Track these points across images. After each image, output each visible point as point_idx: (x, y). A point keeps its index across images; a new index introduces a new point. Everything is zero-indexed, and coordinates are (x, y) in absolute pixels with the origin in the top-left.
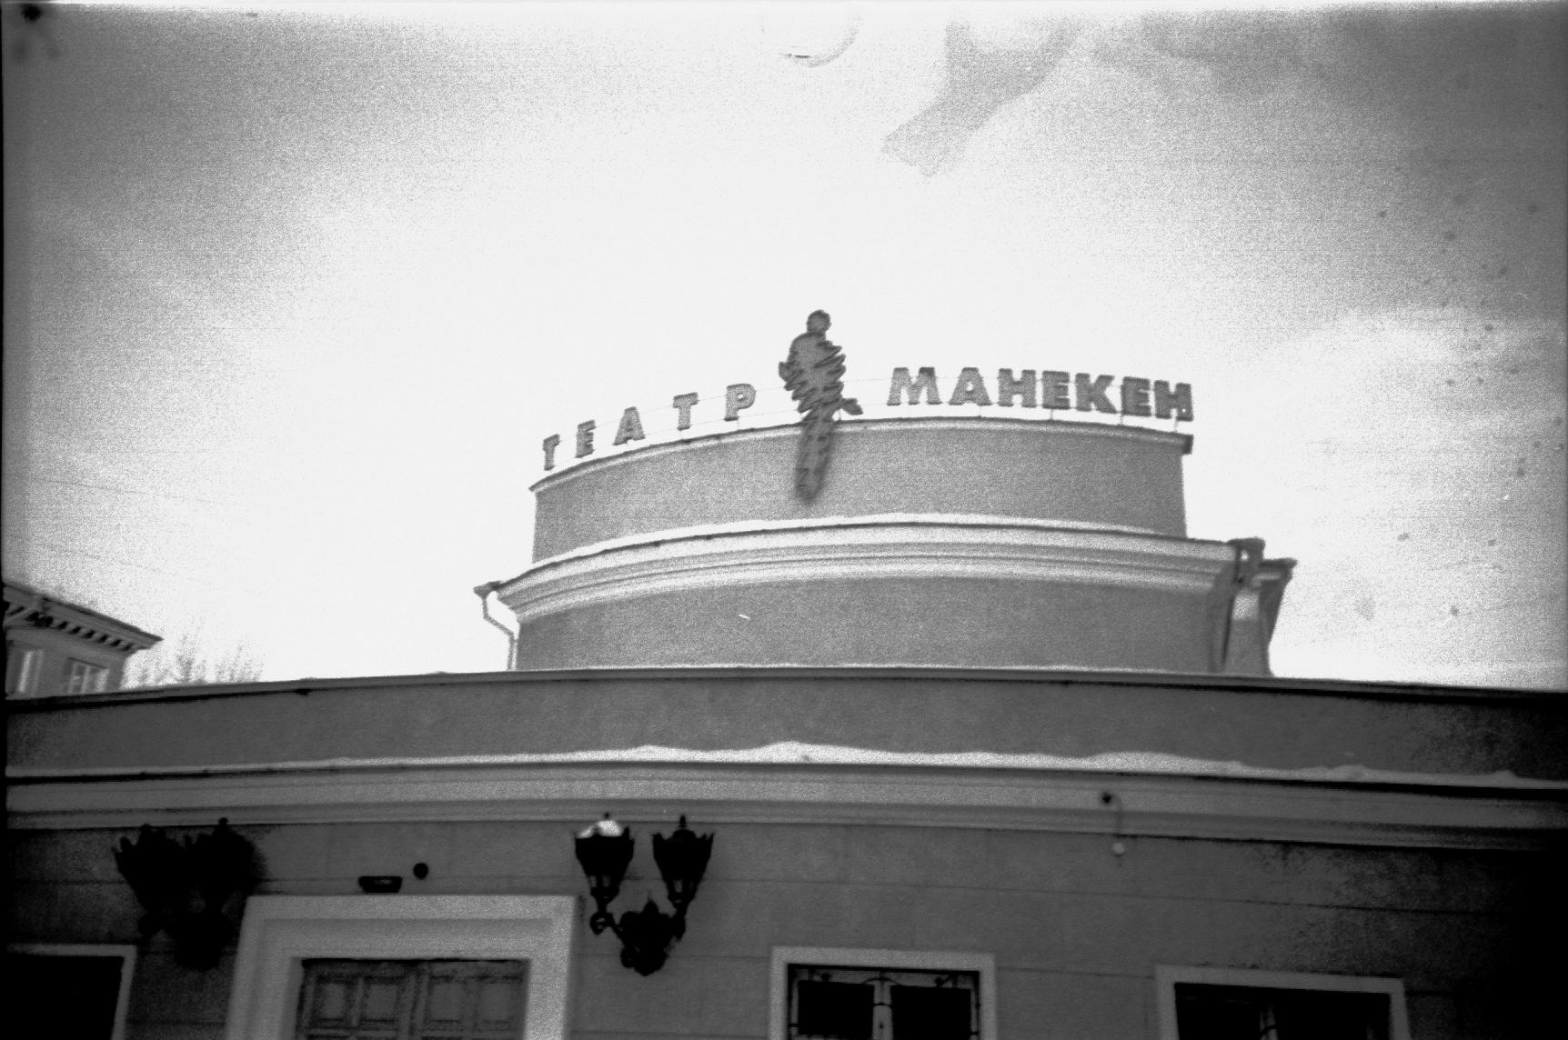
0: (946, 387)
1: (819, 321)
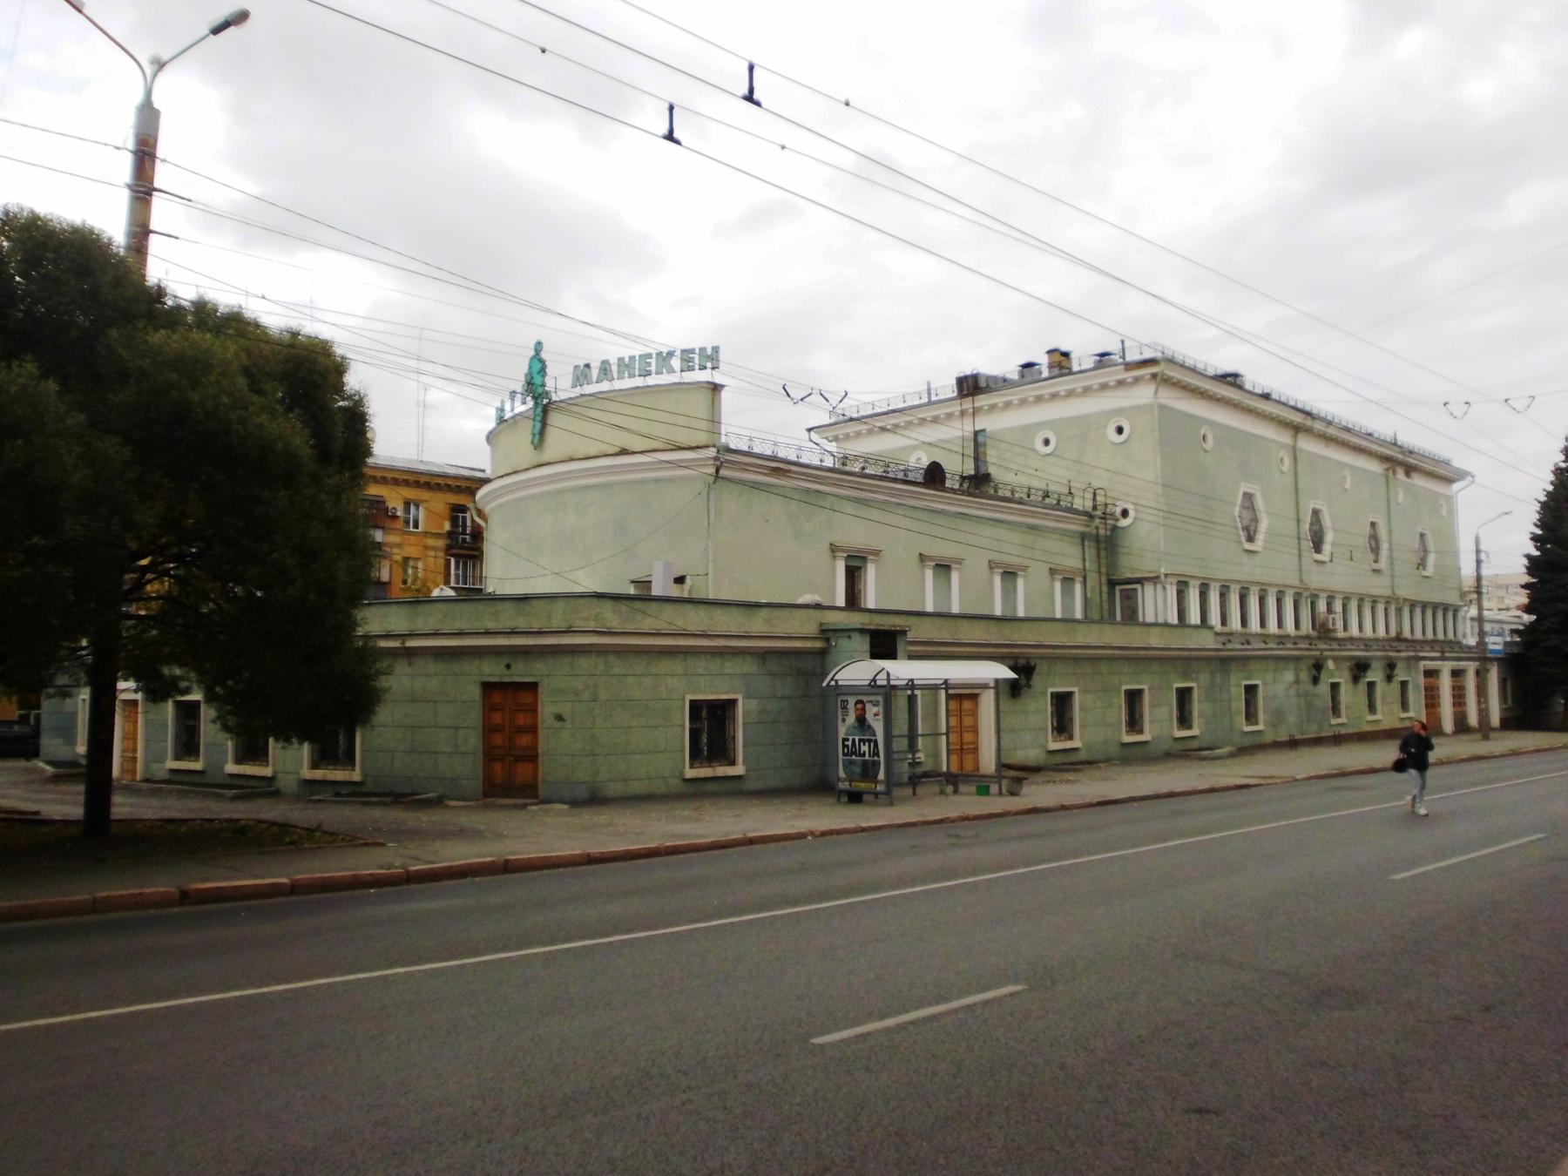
0: (595, 373)
1: (539, 346)
